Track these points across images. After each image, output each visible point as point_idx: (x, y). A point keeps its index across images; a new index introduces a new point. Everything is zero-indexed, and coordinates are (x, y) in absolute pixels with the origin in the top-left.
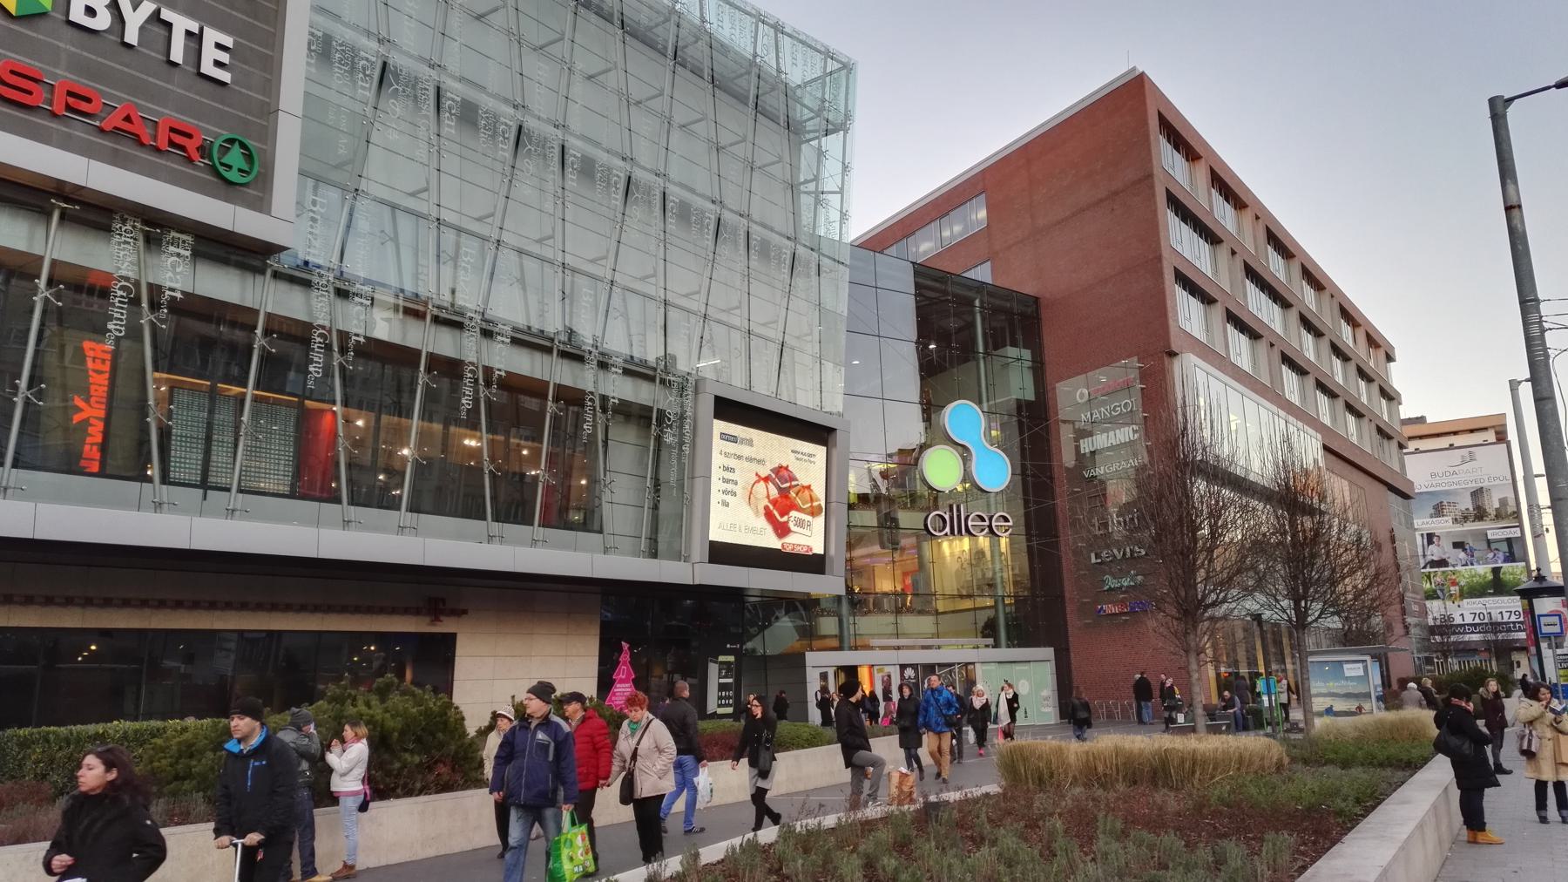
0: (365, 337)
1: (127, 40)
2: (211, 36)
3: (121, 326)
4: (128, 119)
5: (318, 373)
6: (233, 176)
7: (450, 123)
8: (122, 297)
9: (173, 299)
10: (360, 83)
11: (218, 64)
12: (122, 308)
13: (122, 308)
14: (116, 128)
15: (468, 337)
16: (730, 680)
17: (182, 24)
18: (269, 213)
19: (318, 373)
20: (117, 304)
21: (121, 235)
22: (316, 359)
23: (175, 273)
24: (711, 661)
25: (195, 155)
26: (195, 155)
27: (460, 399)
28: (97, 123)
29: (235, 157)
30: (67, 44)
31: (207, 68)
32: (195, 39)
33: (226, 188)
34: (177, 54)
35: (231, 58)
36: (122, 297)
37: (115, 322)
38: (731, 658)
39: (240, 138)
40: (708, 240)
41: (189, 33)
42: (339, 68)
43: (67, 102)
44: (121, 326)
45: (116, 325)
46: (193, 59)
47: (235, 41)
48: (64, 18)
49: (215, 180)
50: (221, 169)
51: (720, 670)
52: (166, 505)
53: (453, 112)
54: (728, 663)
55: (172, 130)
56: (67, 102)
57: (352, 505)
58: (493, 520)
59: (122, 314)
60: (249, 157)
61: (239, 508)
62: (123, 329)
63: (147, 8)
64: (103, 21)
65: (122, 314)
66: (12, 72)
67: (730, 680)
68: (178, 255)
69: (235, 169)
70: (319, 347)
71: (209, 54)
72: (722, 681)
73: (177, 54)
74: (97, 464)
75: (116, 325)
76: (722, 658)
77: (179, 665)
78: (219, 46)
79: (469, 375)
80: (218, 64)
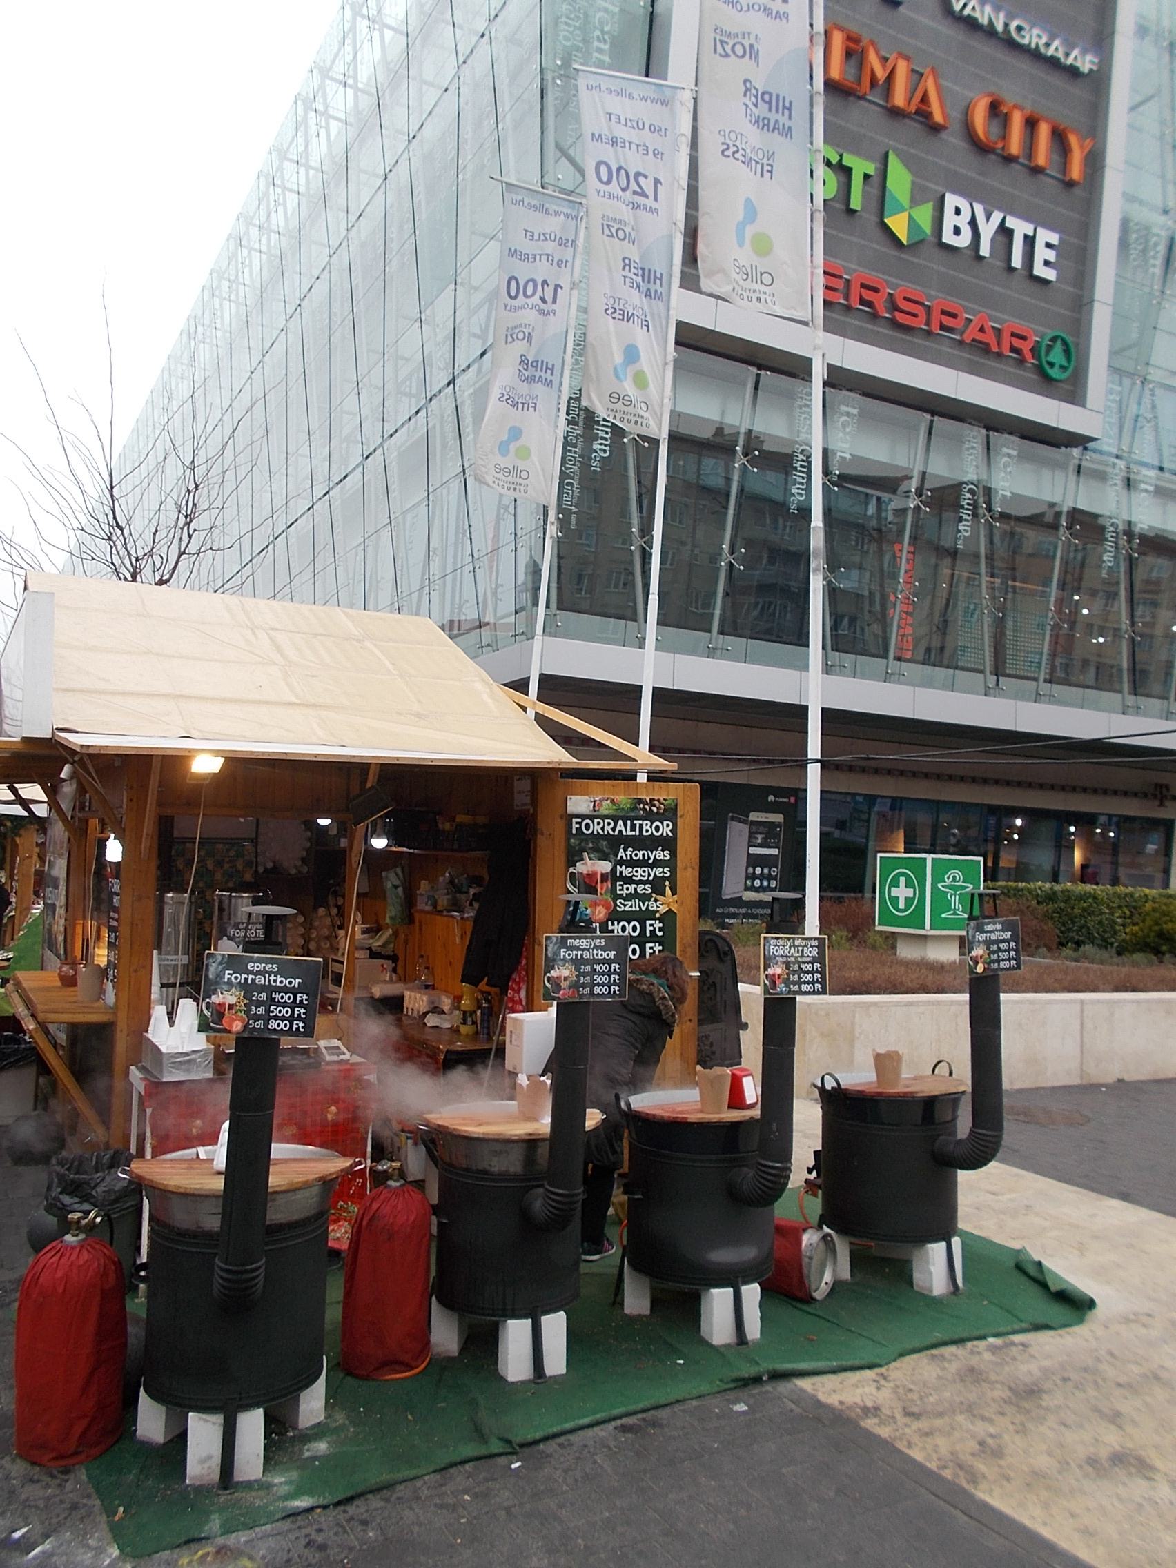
0: (1012, 493)
1: (852, 206)
2: (1045, 236)
3: (606, 445)
4: (982, 330)
5: (605, 451)
6: (1054, 373)
7: (602, 46)
8: (803, 461)
9: (1004, 496)
10: (596, 44)
11: (1047, 263)
12: (803, 472)
13: (803, 472)
14: (973, 340)
15: (968, 449)
16: (775, 852)
17: (1021, 228)
18: (1083, 405)
19: (605, 451)
20: (966, 506)
21: (801, 398)
22: (965, 517)
23: (845, 434)
24: (733, 819)
25: (1028, 355)
26: (1028, 355)
27: (1100, 557)
28: (957, 337)
29: (1057, 356)
30: (936, 264)
31: (1039, 270)
32: (1030, 241)
33: (1045, 383)
34: (1017, 262)
35: (1057, 256)
36: (803, 461)
37: (600, 441)
38: (778, 818)
39: (1063, 335)
40: (1154, 266)
41: (1026, 236)
42: (566, 24)
43: (861, 296)
44: (606, 445)
45: (601, 444)
46: (874, 205)
47: (1061, 239)
48: (843, 207)
49: (1035, 377)
50: (1047, 367)
51: (752, 835)
52: (719, 652)
53: (606, 29)
54: (772, 825)
55: (863, 286)
56: (861, 296)
57: (837, 651)
58: (1130, 693)
59: (607, 433)
60: (1067, 352)
61: (720, 646)
62: (607, 448)
63: (997, 217)
64: (964, 241)
65: (607, 433)
66: (905, 299)
67: (775, 852)
68: (848, 414)
69: (1057, 366)
70: (968, 504)
71: (1041, 254)
72: (753, 850)
73: (1017, 262)
74: (910, 653)
75: (601, 444)
76: (754, 816)
77: (833, 829)
78: (1049, 245)
79: (968, 496)
80: (1047, 263)
